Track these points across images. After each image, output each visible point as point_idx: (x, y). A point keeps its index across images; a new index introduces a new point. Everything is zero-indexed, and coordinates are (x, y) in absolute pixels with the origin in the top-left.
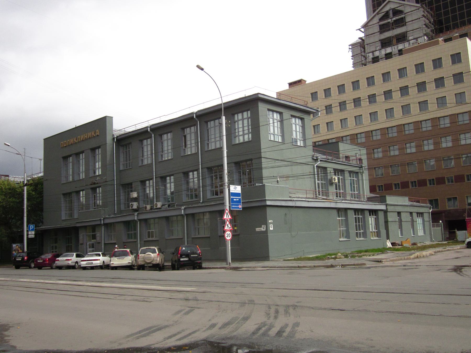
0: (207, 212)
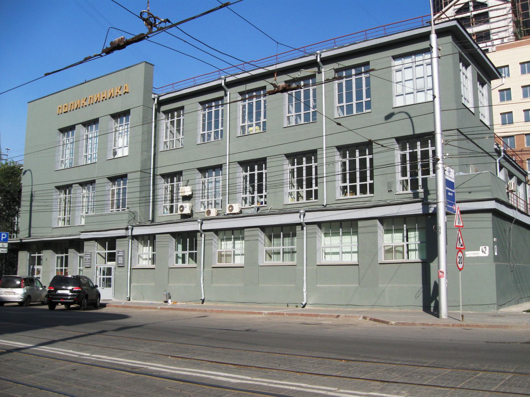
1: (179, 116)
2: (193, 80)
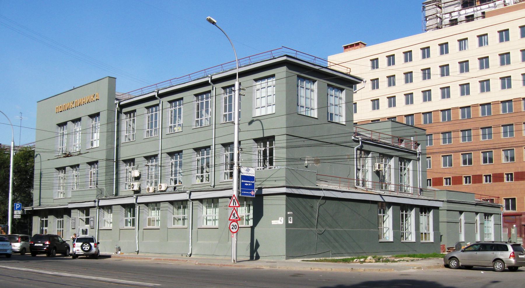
0: (390, 204)
1: (180, 105)
2: (188, 76)
